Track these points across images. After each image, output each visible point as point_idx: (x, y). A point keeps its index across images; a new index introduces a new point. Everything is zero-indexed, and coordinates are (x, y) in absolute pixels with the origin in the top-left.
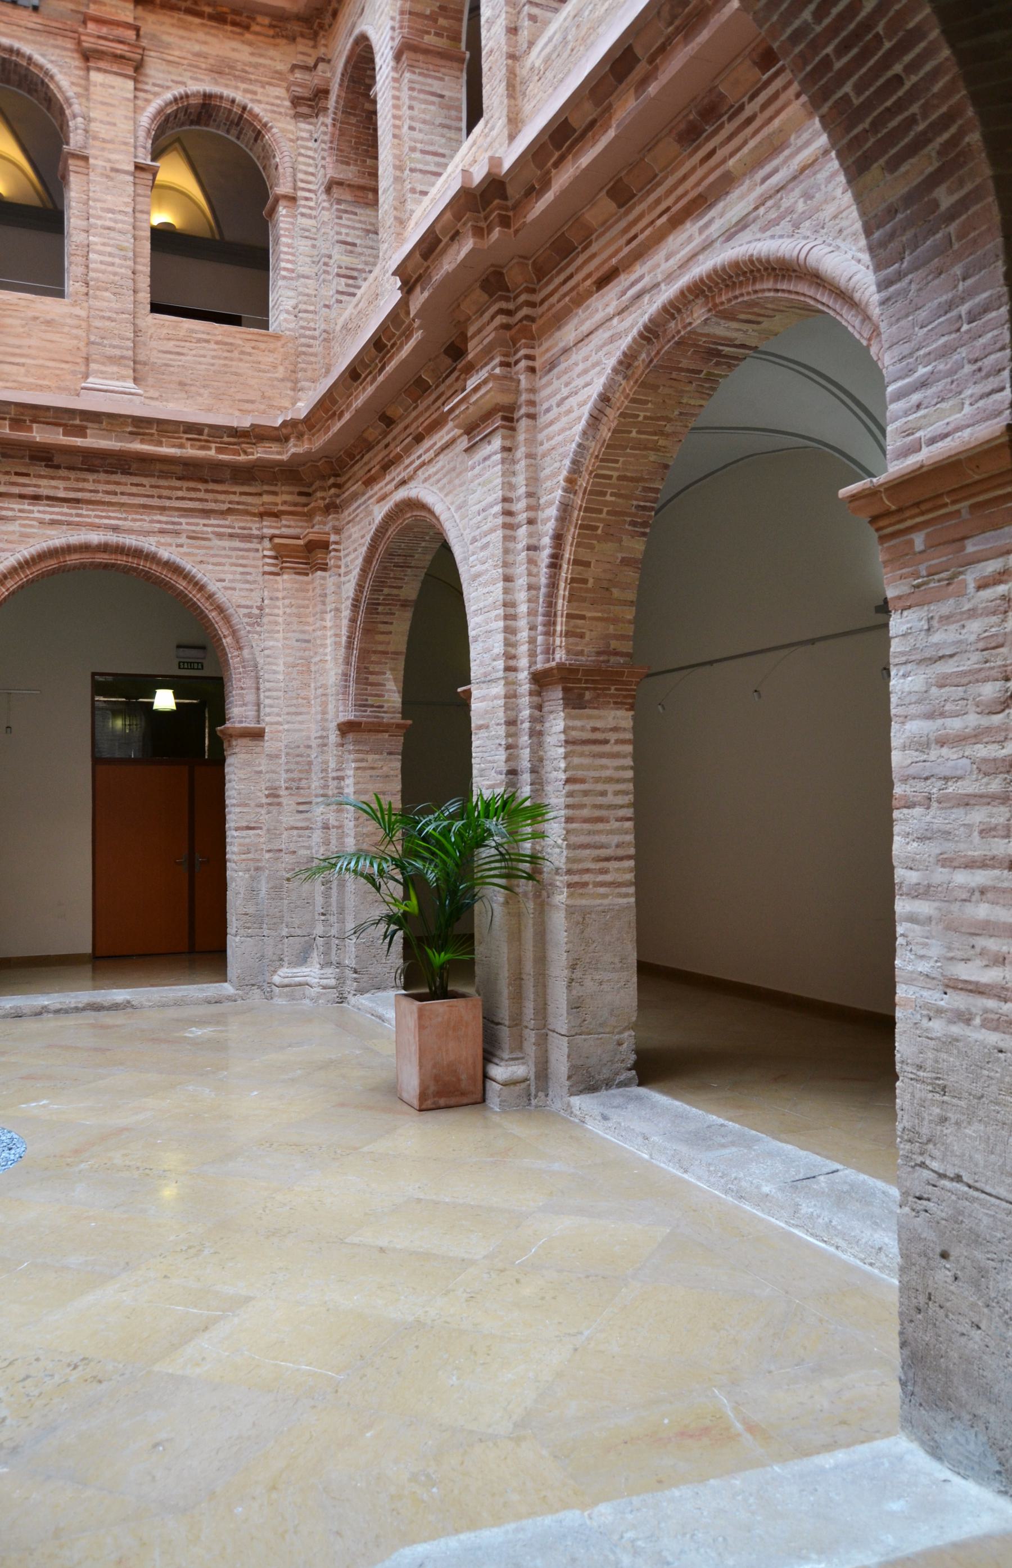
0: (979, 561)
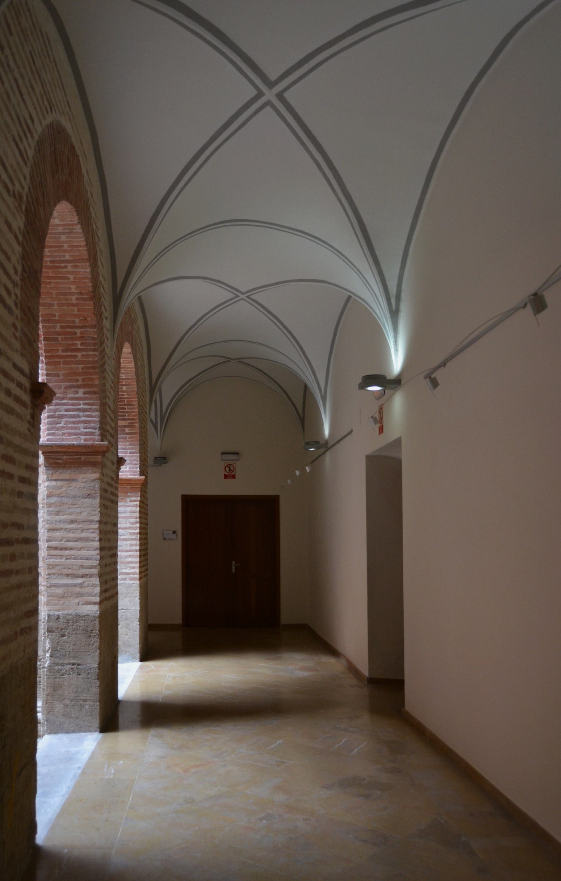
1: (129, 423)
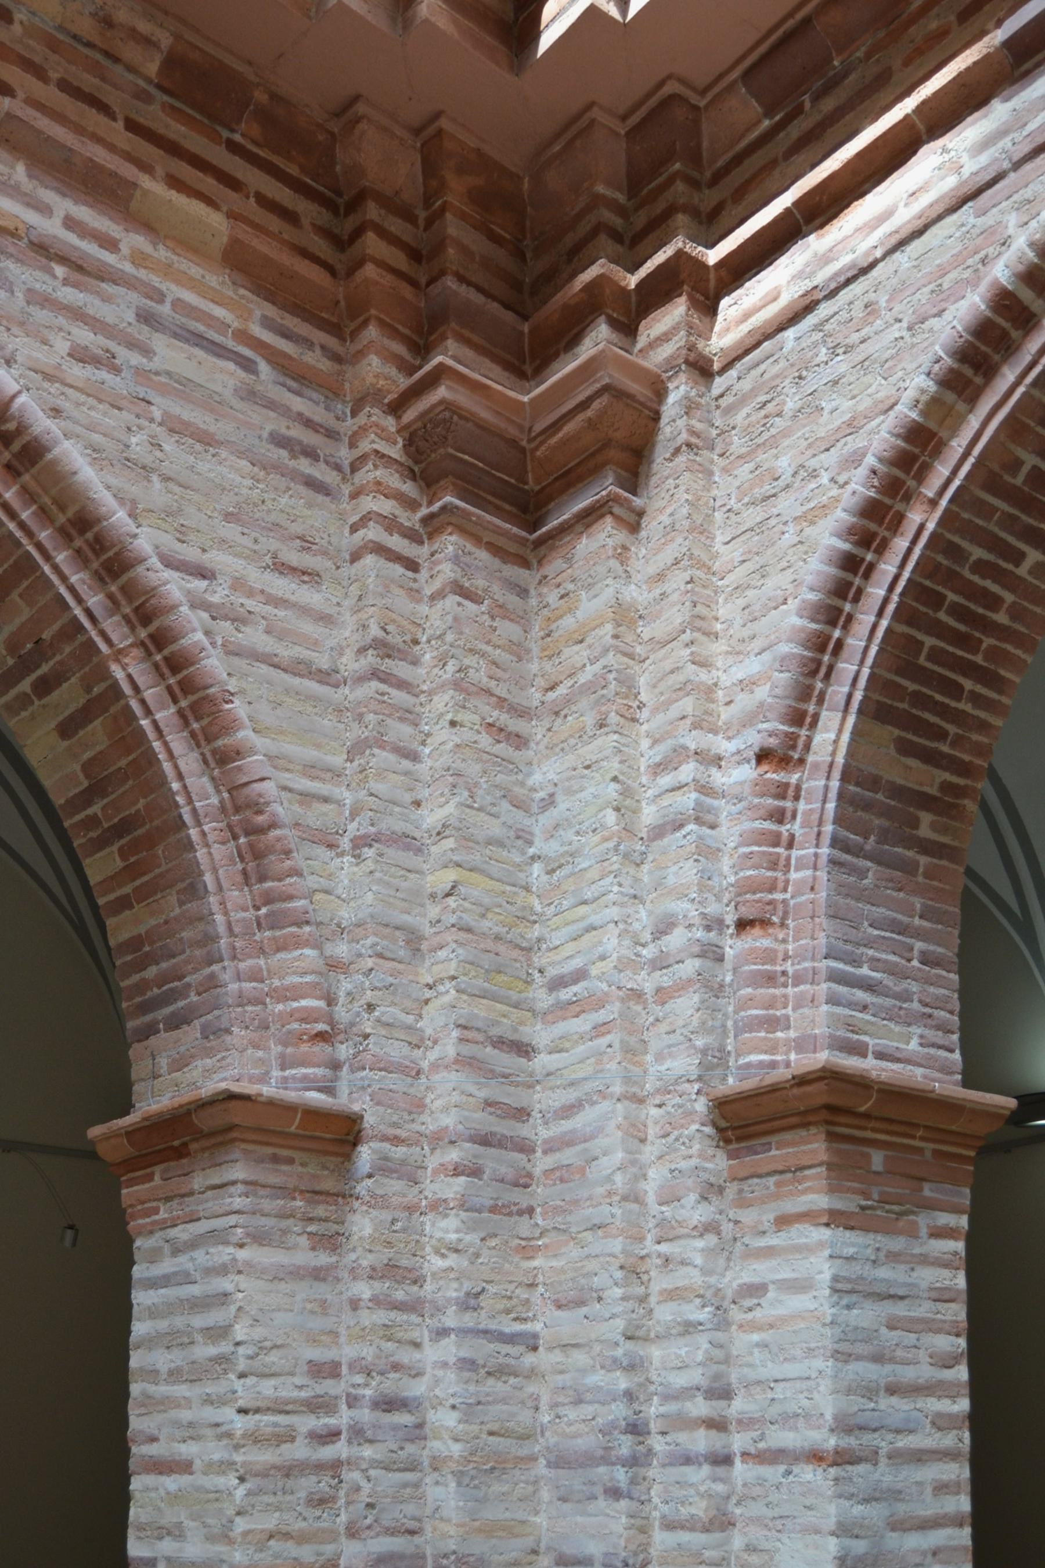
0: (934, 1209)
1: (946, 787)
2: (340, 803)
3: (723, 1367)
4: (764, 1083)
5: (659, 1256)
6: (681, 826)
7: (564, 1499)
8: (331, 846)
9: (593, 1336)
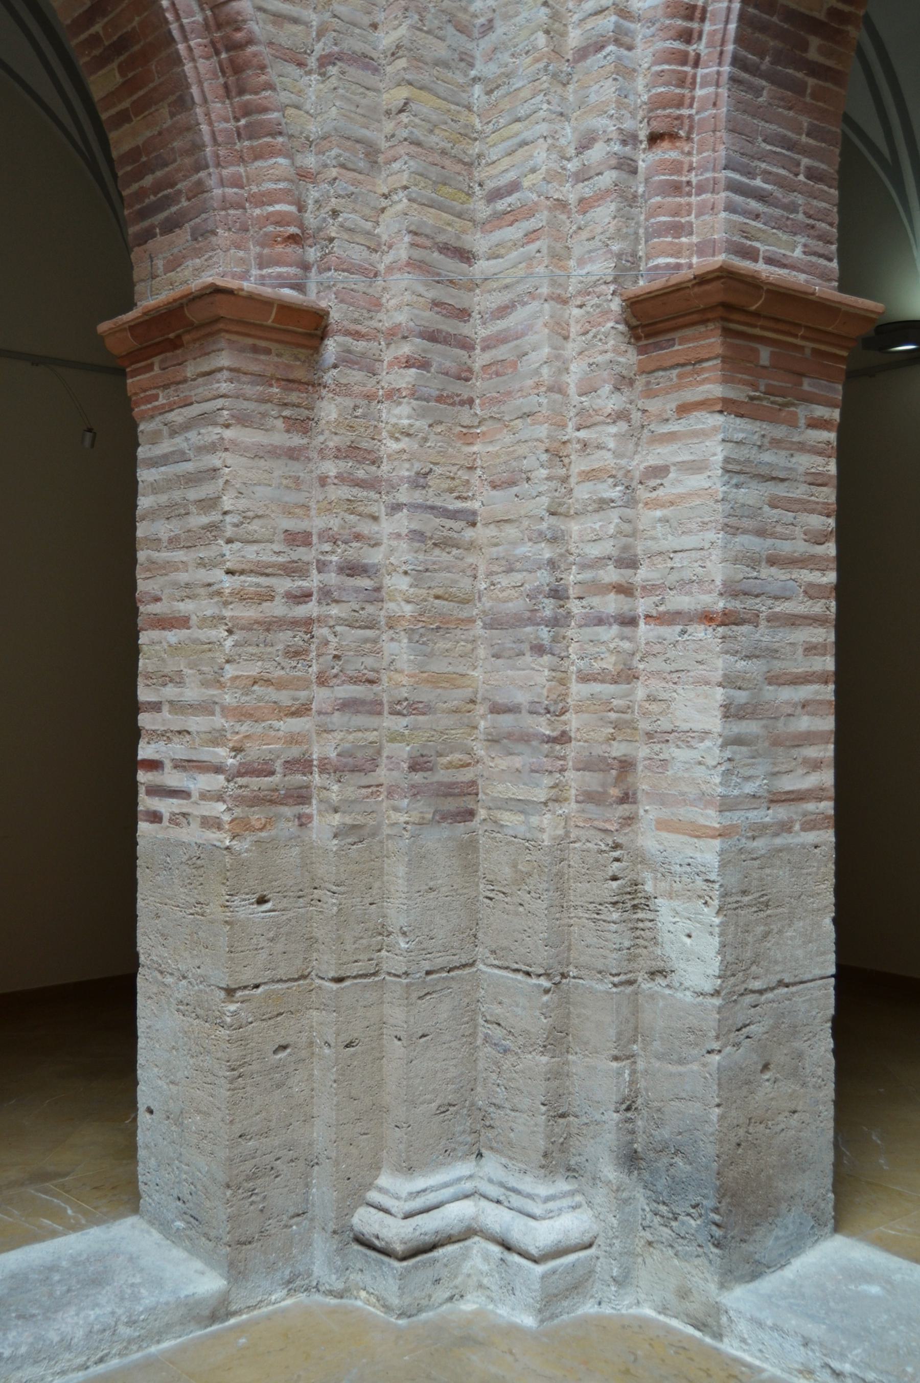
0: (812, 403)
2: (307, 24)
3: (630, 540)
4: (670, 283)
5: (579, 441)
6: (602, 47)
7: (497, 656)
8: (301, 65)
9: (523, 513)
